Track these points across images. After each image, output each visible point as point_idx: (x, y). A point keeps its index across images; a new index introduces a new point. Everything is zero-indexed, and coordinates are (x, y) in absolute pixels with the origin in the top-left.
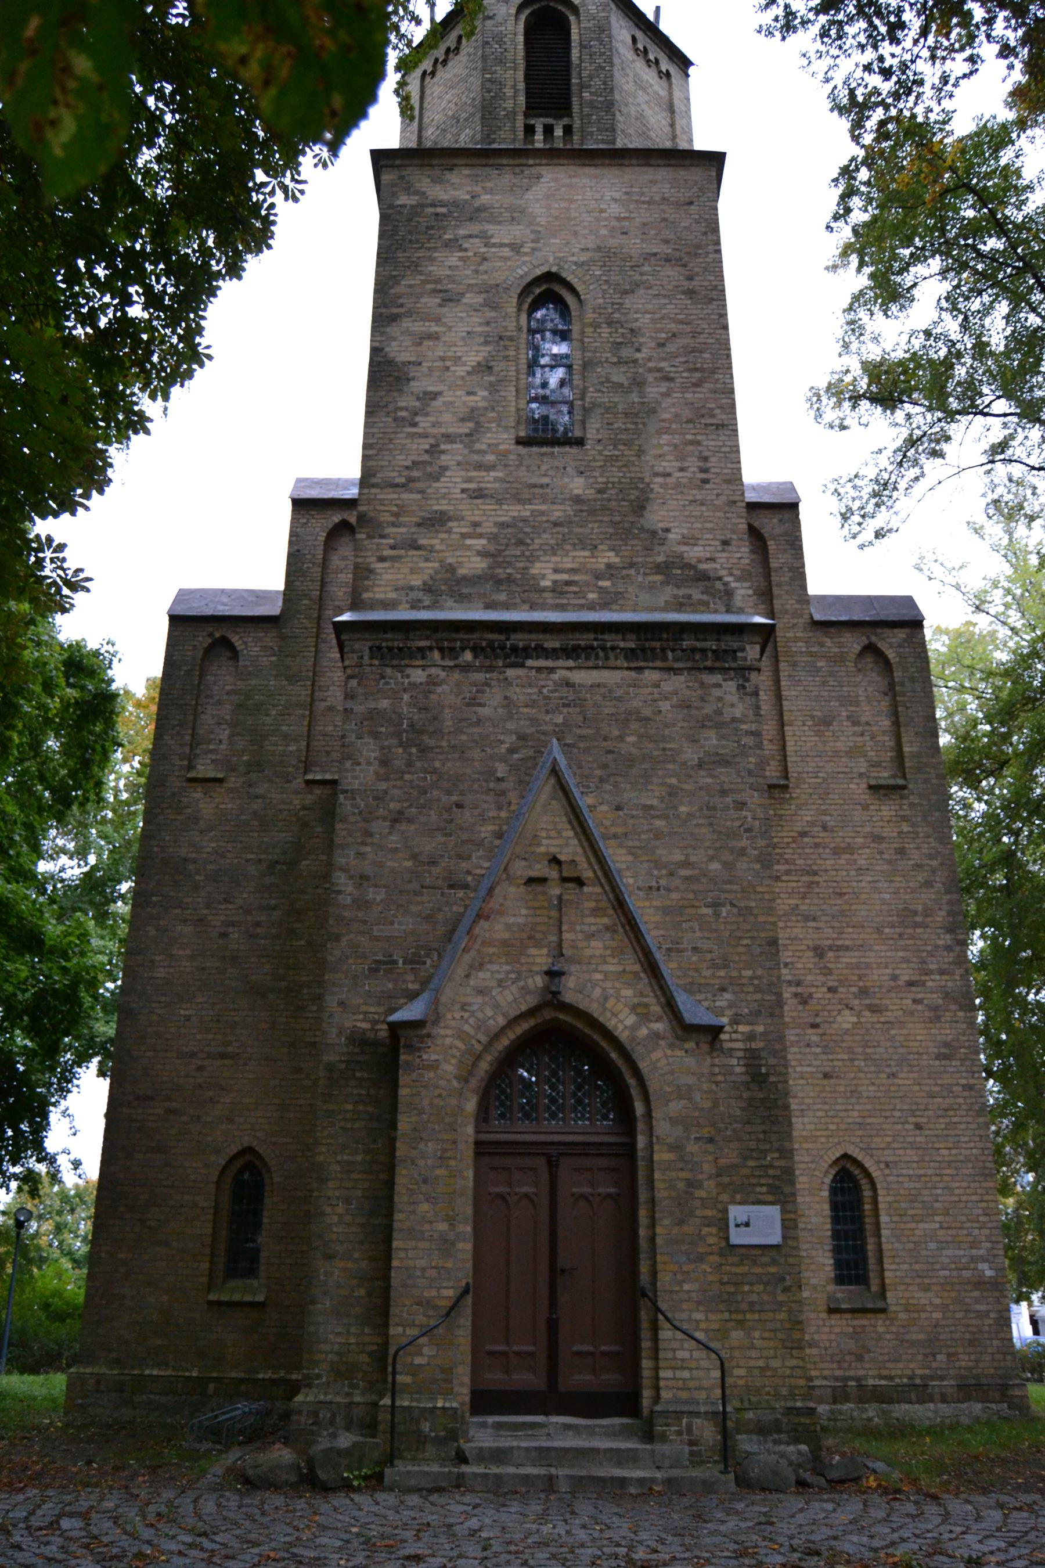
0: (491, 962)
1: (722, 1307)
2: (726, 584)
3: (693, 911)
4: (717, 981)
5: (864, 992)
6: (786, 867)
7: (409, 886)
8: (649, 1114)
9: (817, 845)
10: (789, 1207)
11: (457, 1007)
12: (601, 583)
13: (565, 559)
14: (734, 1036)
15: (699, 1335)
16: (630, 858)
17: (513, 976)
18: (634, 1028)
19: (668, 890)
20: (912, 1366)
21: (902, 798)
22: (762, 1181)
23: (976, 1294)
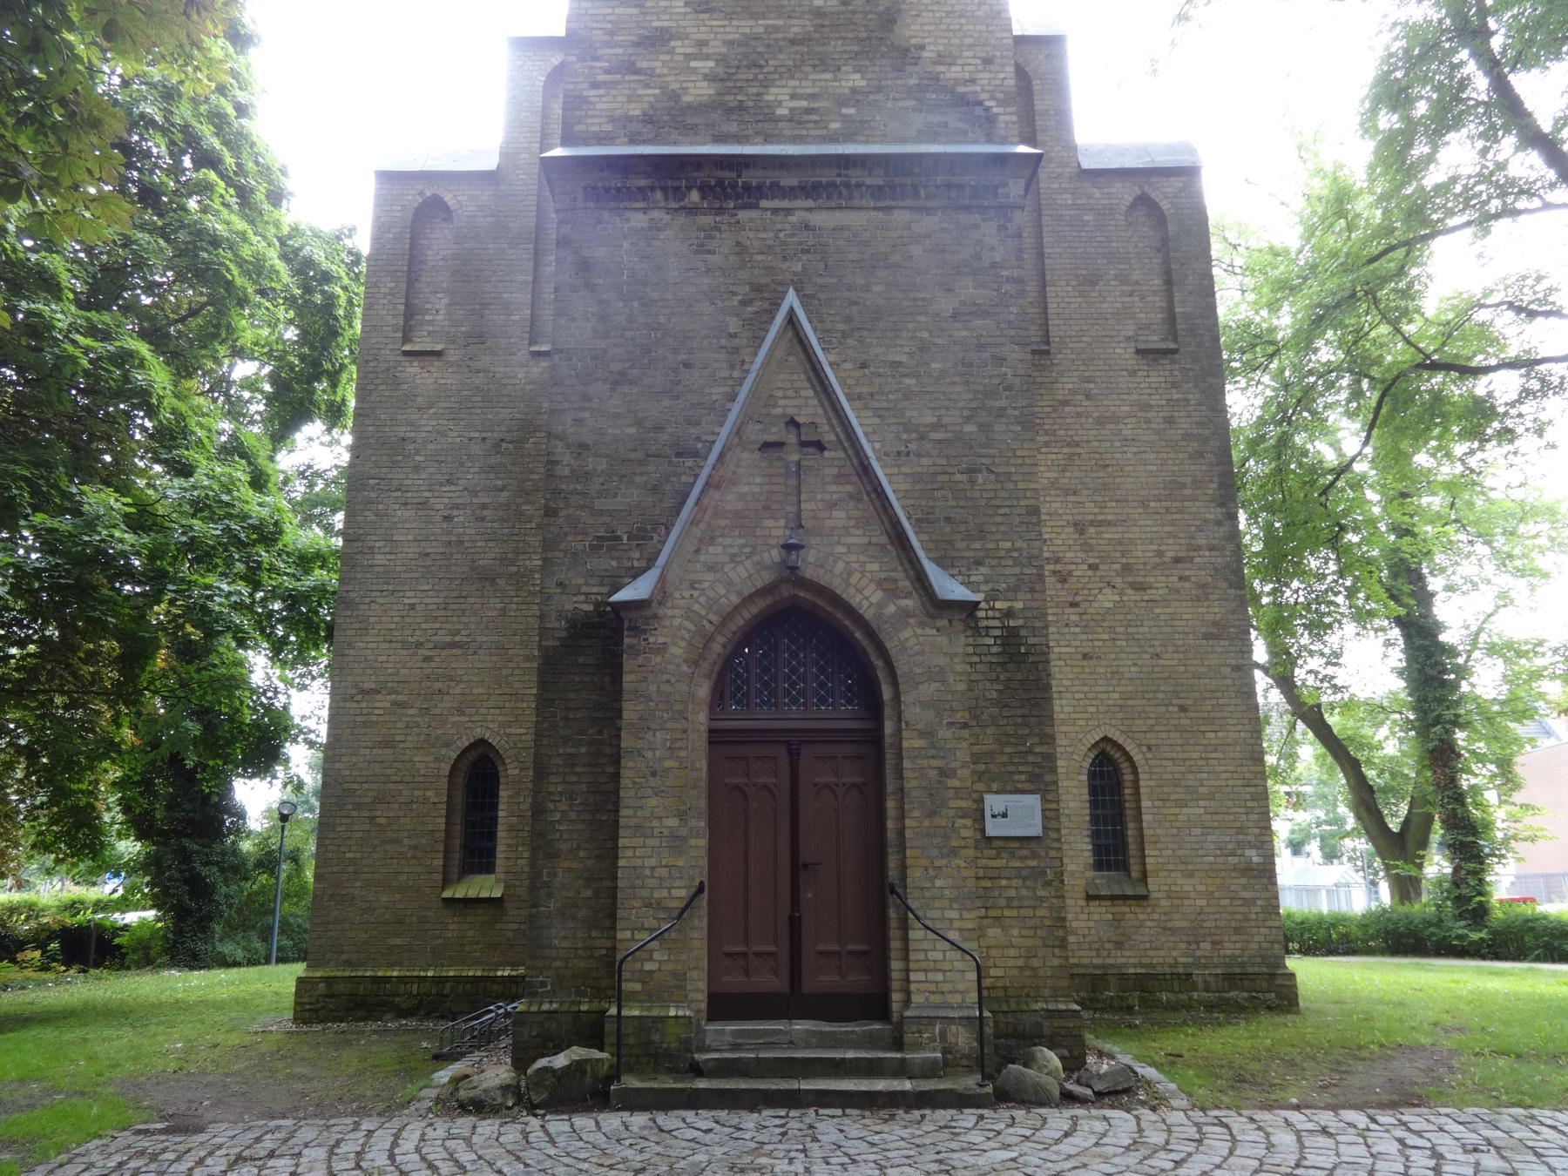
0: (722, 535)
1: (978, 903)
2: (987, 109)
3: (946, 478)
4: (972, 554)
5: (1127, 568)
6: (1046, 438)
7: (633, 455)
8: (897, 697)
9: (1079, 415)
10: (1049, 797)
11: (686, 585)
12: (844, 111)
13: (804, 83)
14: (990, 613)
15: (953, 935)
16: (877, 421)
17: (747, 550)
18: (880, 605)
19: (919, 455)
20: (1175, 953)
21: (1173, 362)
22: (1021, 768)
23: (1243, 881)
